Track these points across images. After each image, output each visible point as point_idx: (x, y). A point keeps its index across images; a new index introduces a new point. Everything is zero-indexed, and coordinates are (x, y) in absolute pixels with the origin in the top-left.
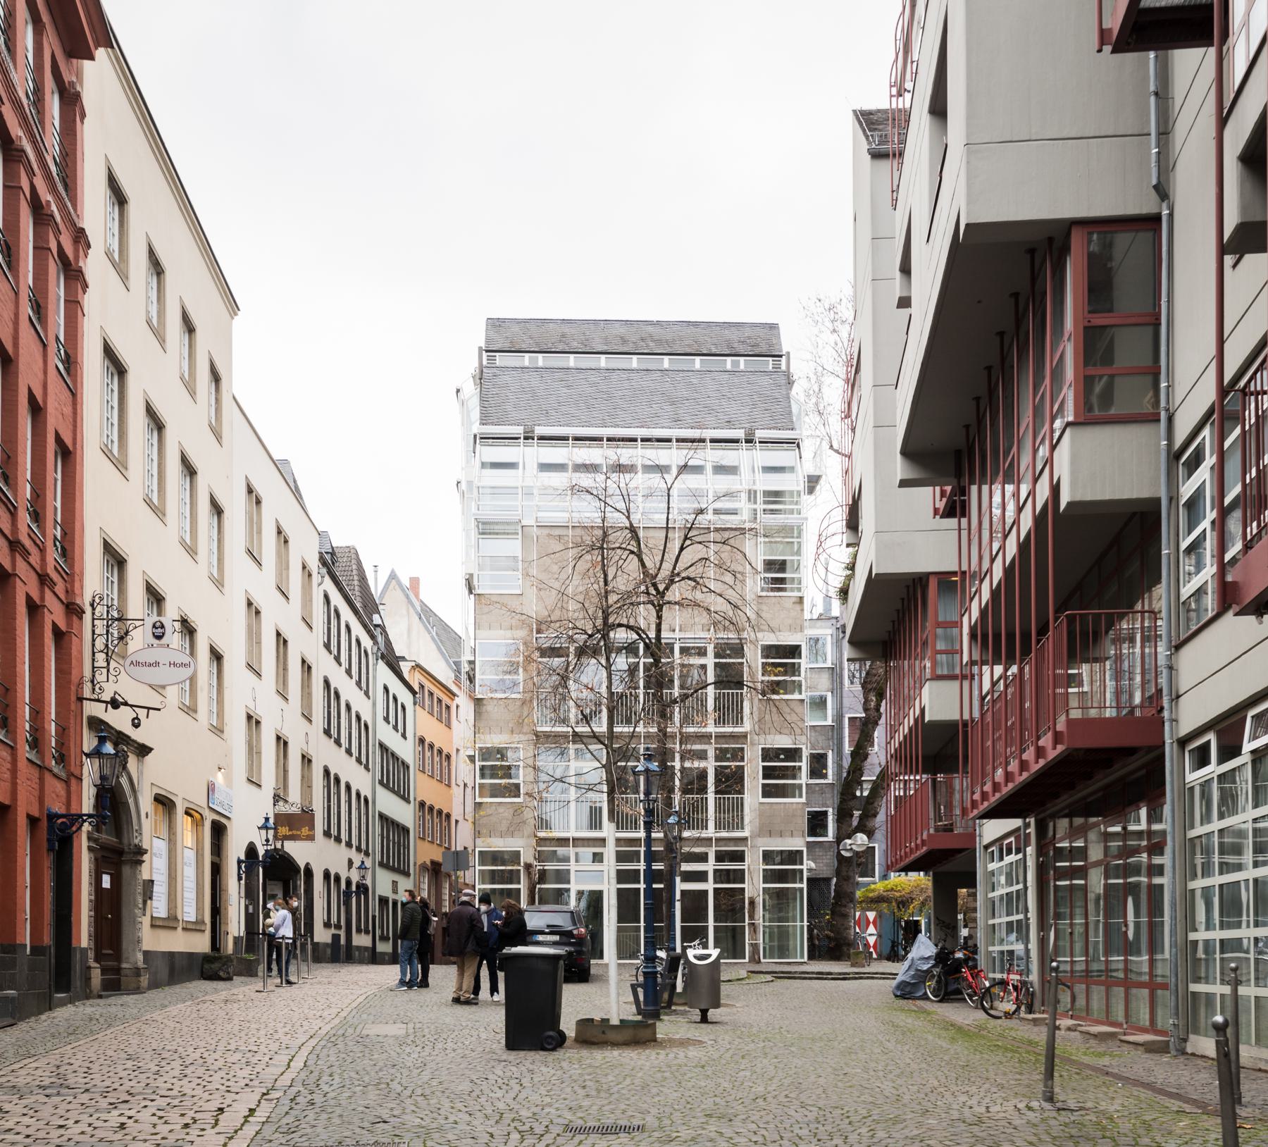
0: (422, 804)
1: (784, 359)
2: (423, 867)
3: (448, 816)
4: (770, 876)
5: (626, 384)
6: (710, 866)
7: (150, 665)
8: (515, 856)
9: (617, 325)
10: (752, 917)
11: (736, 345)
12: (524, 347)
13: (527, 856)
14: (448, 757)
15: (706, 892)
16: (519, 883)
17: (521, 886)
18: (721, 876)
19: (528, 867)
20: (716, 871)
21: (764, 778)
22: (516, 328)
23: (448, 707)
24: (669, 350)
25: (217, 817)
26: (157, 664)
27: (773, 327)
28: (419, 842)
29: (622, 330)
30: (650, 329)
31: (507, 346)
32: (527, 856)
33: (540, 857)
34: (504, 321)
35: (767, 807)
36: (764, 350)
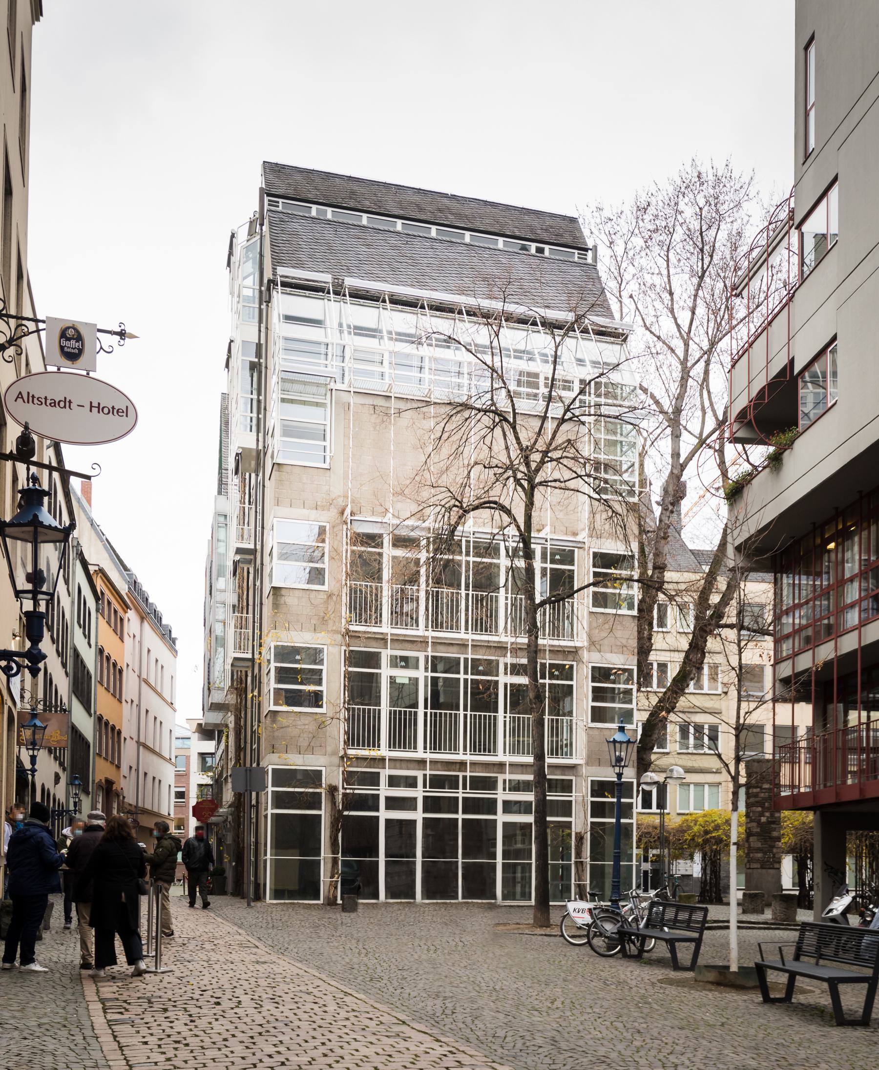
0: (100, 719)
1: (590, 253)
2: (100, 786)
3: (119, 732)
4: (598, 810)
5: (431, 253)
6: (418, 793)
7: (54, 404)
8: (314, 777)
9: (410, 192)
10: (579, 854)
11: (539, 232)
12: (310, 196)
13: (333, 776)
14: (121, 671)
15: (414, 822)
16: (320, 809)
17: (322, 812)
18: (431, 804)
19: (333, 790)
20: (425, 798)
21: (593, 700)
22: (298, 177)
23: (122, 620)
24: (470, 226)
25: (664, 630)
26: (67, 403)
27: (573, 220)
28: (97, 758)
29: (416, 198)
30: (446, 201)
31: (291, 192)
32: (333, 776)
33: (349, 778)
34: (284, 167)
35: (596, 732)
36: (567, 239)
